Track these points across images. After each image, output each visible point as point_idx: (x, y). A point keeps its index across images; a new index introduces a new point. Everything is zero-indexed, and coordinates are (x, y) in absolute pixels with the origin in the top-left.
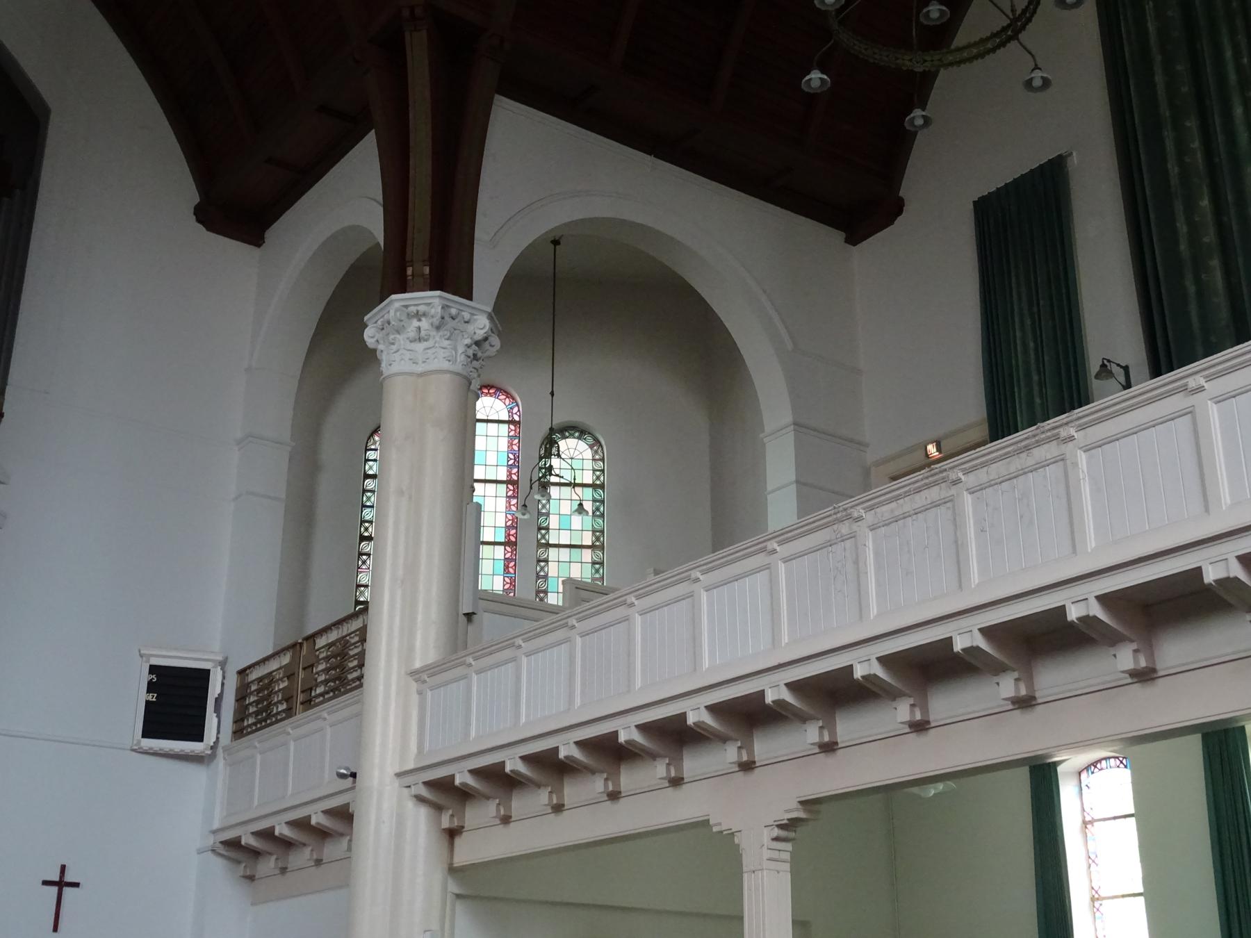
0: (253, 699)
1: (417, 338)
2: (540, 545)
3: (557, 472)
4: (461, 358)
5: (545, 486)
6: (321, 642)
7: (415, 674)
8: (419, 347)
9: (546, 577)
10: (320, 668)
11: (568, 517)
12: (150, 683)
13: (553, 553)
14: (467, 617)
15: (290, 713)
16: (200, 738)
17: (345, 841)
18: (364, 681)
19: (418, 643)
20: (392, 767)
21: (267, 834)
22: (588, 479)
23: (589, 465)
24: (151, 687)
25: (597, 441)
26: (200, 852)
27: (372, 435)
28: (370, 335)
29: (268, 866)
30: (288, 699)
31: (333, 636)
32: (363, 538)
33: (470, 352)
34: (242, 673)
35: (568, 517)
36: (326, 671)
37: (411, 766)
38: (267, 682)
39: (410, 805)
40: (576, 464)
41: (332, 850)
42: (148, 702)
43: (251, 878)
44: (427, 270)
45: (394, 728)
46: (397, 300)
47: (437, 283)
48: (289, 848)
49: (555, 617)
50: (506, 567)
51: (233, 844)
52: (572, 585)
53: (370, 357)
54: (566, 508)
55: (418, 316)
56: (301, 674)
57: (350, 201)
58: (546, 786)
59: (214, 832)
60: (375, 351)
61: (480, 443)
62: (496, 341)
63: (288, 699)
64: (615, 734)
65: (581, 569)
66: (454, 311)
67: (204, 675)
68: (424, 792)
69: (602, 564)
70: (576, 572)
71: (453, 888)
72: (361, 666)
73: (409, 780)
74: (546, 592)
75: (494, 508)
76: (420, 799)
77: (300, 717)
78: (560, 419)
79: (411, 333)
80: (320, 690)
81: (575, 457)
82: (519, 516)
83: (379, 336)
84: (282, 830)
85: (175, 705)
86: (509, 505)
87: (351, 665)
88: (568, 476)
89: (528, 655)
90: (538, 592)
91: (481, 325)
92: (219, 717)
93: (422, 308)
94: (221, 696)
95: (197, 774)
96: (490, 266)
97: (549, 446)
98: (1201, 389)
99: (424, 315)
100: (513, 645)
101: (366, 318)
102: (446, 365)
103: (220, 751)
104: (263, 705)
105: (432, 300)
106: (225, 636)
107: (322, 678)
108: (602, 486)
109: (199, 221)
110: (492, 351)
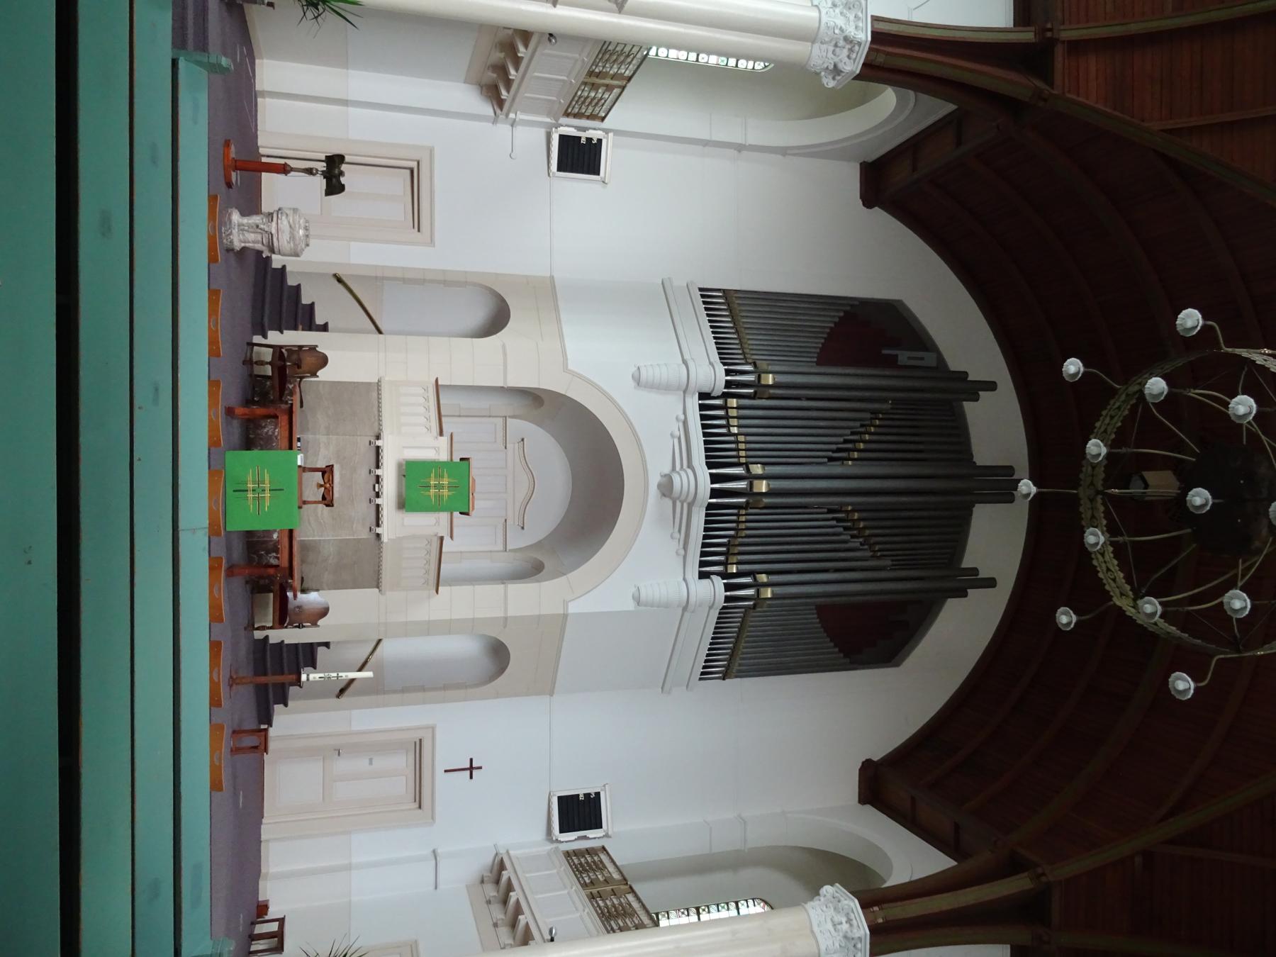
15: (584, 885)
24: (587, 795)
43: (482, 882)
51: (502, 866)
67: (598, 825)
85: (579, 812)
104: (586, 866)
106: (624, 835)
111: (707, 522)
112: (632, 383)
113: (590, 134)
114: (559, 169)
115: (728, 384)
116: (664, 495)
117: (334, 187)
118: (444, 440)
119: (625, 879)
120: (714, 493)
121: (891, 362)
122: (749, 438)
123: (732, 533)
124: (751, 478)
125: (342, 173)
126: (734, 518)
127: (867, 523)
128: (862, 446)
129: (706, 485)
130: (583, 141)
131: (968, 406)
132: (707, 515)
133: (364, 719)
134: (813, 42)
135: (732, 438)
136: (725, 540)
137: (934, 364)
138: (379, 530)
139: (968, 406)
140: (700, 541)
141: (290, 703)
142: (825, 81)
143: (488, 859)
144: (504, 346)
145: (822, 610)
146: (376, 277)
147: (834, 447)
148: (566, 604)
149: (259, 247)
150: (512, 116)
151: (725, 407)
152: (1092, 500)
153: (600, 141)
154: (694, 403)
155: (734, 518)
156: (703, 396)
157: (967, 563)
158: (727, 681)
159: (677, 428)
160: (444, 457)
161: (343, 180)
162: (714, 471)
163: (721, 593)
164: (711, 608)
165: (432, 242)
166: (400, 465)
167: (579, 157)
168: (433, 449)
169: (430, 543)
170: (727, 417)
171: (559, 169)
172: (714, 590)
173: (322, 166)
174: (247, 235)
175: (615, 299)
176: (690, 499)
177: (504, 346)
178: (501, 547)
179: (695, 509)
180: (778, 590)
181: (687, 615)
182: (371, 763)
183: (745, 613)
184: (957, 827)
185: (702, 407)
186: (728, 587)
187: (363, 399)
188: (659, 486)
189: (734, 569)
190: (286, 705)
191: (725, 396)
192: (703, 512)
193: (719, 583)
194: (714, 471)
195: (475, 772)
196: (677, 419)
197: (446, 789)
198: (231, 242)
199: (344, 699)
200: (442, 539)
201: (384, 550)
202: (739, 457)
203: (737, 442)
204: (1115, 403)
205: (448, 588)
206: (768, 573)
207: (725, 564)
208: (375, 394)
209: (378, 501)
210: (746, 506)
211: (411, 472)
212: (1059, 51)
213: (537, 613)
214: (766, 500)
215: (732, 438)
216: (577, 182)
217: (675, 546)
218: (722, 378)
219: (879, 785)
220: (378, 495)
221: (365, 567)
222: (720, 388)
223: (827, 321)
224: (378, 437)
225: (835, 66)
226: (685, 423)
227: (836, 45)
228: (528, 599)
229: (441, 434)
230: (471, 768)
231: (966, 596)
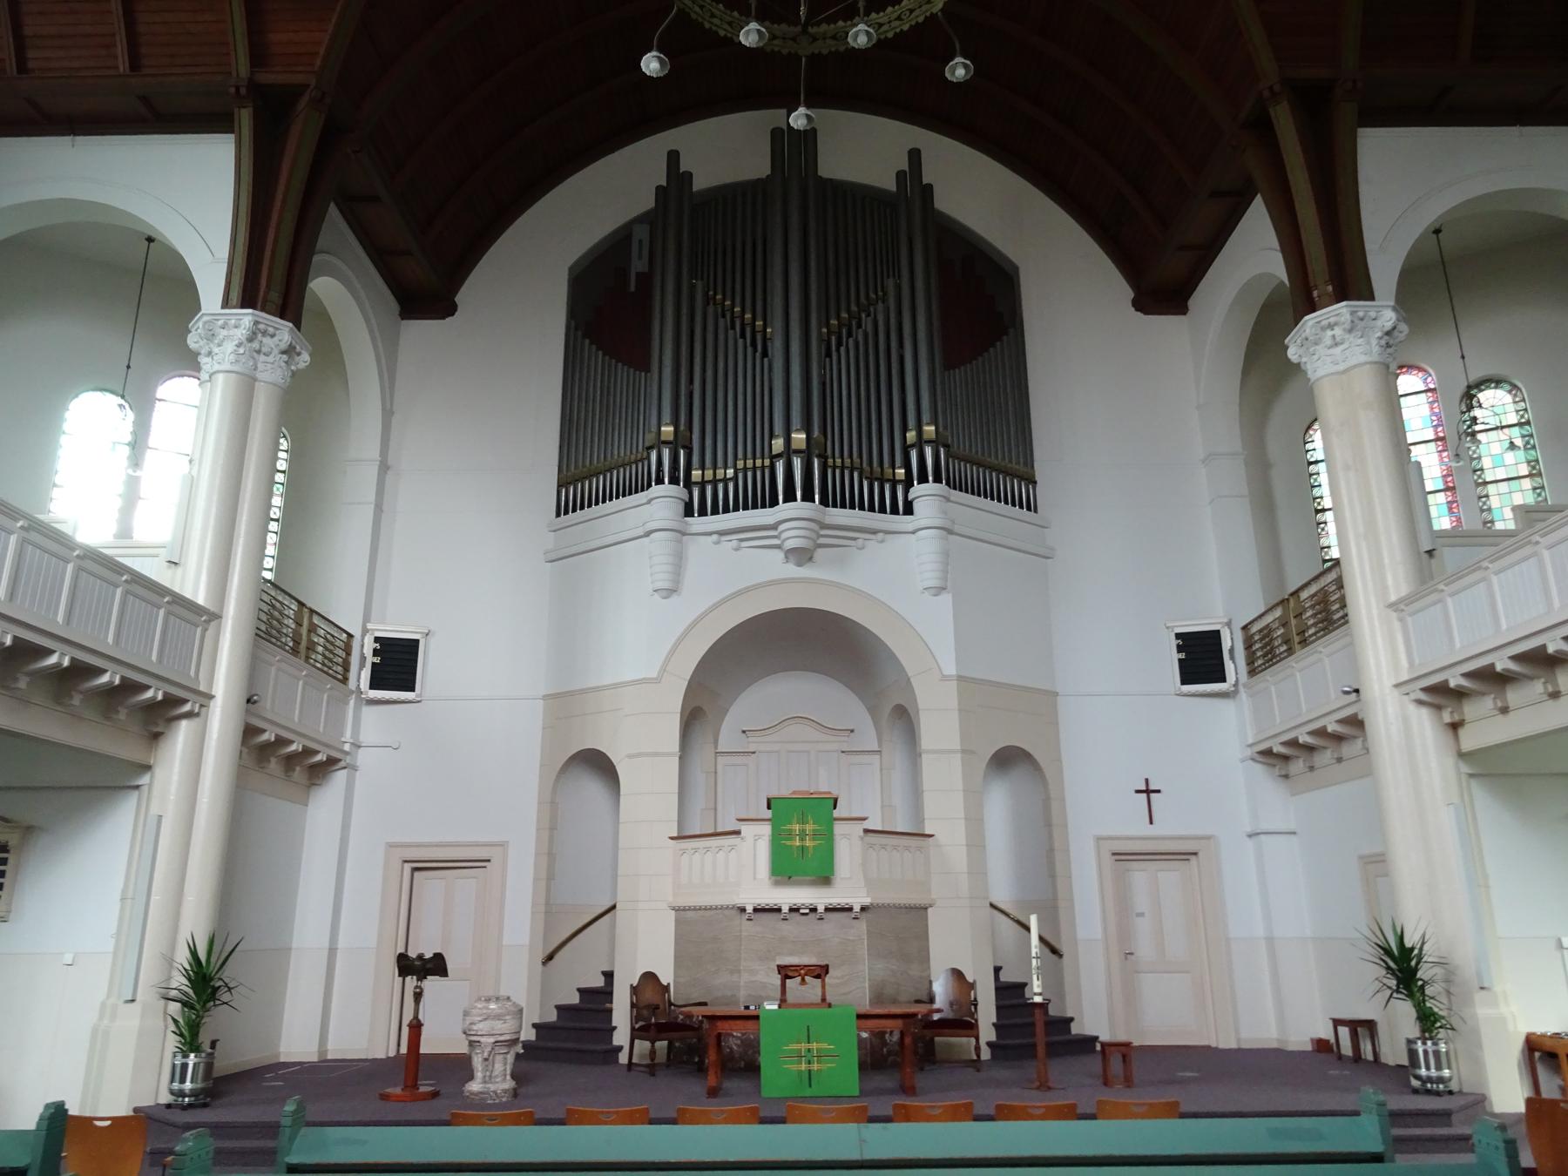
0: (1258, 646)
1: (1333, 345)
2: (1478, 485)
4: (1376, 349)
5: (1473, 434)
6: (1304, 595)
7: (1392, 606)
8: (1338, 350)
9: (1489, 509)
10: (1310, 612)
11: (1500, 455)
13: (1491, 489)
14: (1429, 557)
15: (1290, 651)
16: (1223, 680)
17: (1359, 742)
18: (1351, 617)
19: (1390, 581)
20: (1389, 682)
21: (1293, 743)
22: (1513, 419)
23: (1511, 407)
24: (1180, 649)
25: (1515, 387)
26: (1243, 761)
27: (1309, 427)
28: (1293, 353)
29: (1298, 766)
30: (1286, 642)
31: (1313, 589)
32: (1318, 511)
33: (1383, 342)
34: (1245, 628)
35: (1500, 455)
36: (1314, 616)
37: (1405, 677)
38: (1267, 632)
39: (1412, 709)
40: (1498, 410)
41: (1347, 750)
43: (1286, 776)
44: (1330, 288)
45: (1383, 652)
46: (1310, 320)
47: (1341, 295)
48: (1317, 751)
49: (1513, 540)
50: (1450, 509)
51: (1268, 753)
52: (1521, 511)
53: (1297, 368)
54: (1496, 449)
55: (1331, 326)
56: (1293, 622)
57: (1254, 253)
58: (1539, 678)
60: (1298, 365)
61: (1406, 414)
62: (1404, 327)
63: (1286, 642)
64: (1544, 647)
65: (1524, 494)
66: (1361, 314)
67: (1216, 635)
68: (1423, 696)
69: (1543, 488)
70: (1518, 500)
71: (1465, 769)
72: (1344, 606)
74: (1492, 522)
75: (1431, 463)
76: (1420, 702)
77: (1300, 652)
78: (1474, 376)
79: (1329, 342)
80: (1311, 631)
81: (1496, 404)
82: (1454, 464)
83: (1301, 351)
84: (1278, 749)
85: (1200, 658)
86: (1441, 459)
87: (1334, 608)
88: (1494, 422)
89: (1496, 574)
90: (1485, 523)
91: (1388, 318)
93: (1332, 320)
95: (1226, 706)
96: (1384, 267)
97: (1469, 398)
98: (1537, 543)
99: (1336, 324)
100: (1480, 568)
102: (1363, 359)
103: (1241, 688)
104: (1266, 650)
105: (1341, 311)
106: (1228, 603)
107: (1311, 622)
108: (1528, 423)
110: (1402, 337)
111: (843, 506)
112: (675, 598)
113: (368, 651)
114: (412, 689)
115: (674, 480)
116: (811, 559)
117: (436, 966)
118: (746, 829)
120: (809, 497)
121: (645, 280)
122: (740, 455)
124: (788, 453)
125: (420, 957)
127: (843, 306)
129: (798, 508)
130: (377, 660)
132: (835, 506)
138: (857, 908)
140: (866, 514)
141: (1069, 1014)
142: (302, 365)
144: (630, 756)
147: (750, 350)
148: (945, 678)
151: (702, 485)
153: (377, 639)
154: (697, 523)
156: (688, 512)
157: (890, 185)
159: (729, 543)
160: (766, 830)
161: (428, 955)
162: (781, 498)
163: (930, 487)
164: (948, 500)
165: (503, 845)
166: (777, 883)
167: (397, 664)
168: (757, 842)
169: (871, 846)
170: (715, 482)
171: (412, 689)
172: (926, 495)
174: (496, 1073)
175: (570, 619)
177: (630, 756)
179: (828, 520)
180: (926, 417)
181: (956, 528)
183: (954, 457)
185: (703, 513)
186: (923, 479)
187: (697, 928)
188: (799, 565)
189: (901, 472)
190: (1072, 1019)
191: (688, 484)
193: (917, 490)
194: (781, 498)
195: (1152, 787)
197: (1172, 824)
198: (505, 1091)
200: (867, 831)
201: (880, 902)
203: (745, 469)
206: (905, 429)
207: (894, 483)
208: (690, 914)
209: (821, 909)
210: (823, 457)
211: (784, 869)
212: (265, 78)
213: (956, 713)
215: (740, 476)
216: (428, 667)
217: (872, 544)
218: (666, 488)
219: (1163, 290)
220: (814, 910)
221: (903, 925)
222: (679, 491)
224: (743, 910)
225: (283, 352)
226: (722, 533)
227: (259, 352)
228: (940, 725)
229: (738, 833)
230: (1148, 792)
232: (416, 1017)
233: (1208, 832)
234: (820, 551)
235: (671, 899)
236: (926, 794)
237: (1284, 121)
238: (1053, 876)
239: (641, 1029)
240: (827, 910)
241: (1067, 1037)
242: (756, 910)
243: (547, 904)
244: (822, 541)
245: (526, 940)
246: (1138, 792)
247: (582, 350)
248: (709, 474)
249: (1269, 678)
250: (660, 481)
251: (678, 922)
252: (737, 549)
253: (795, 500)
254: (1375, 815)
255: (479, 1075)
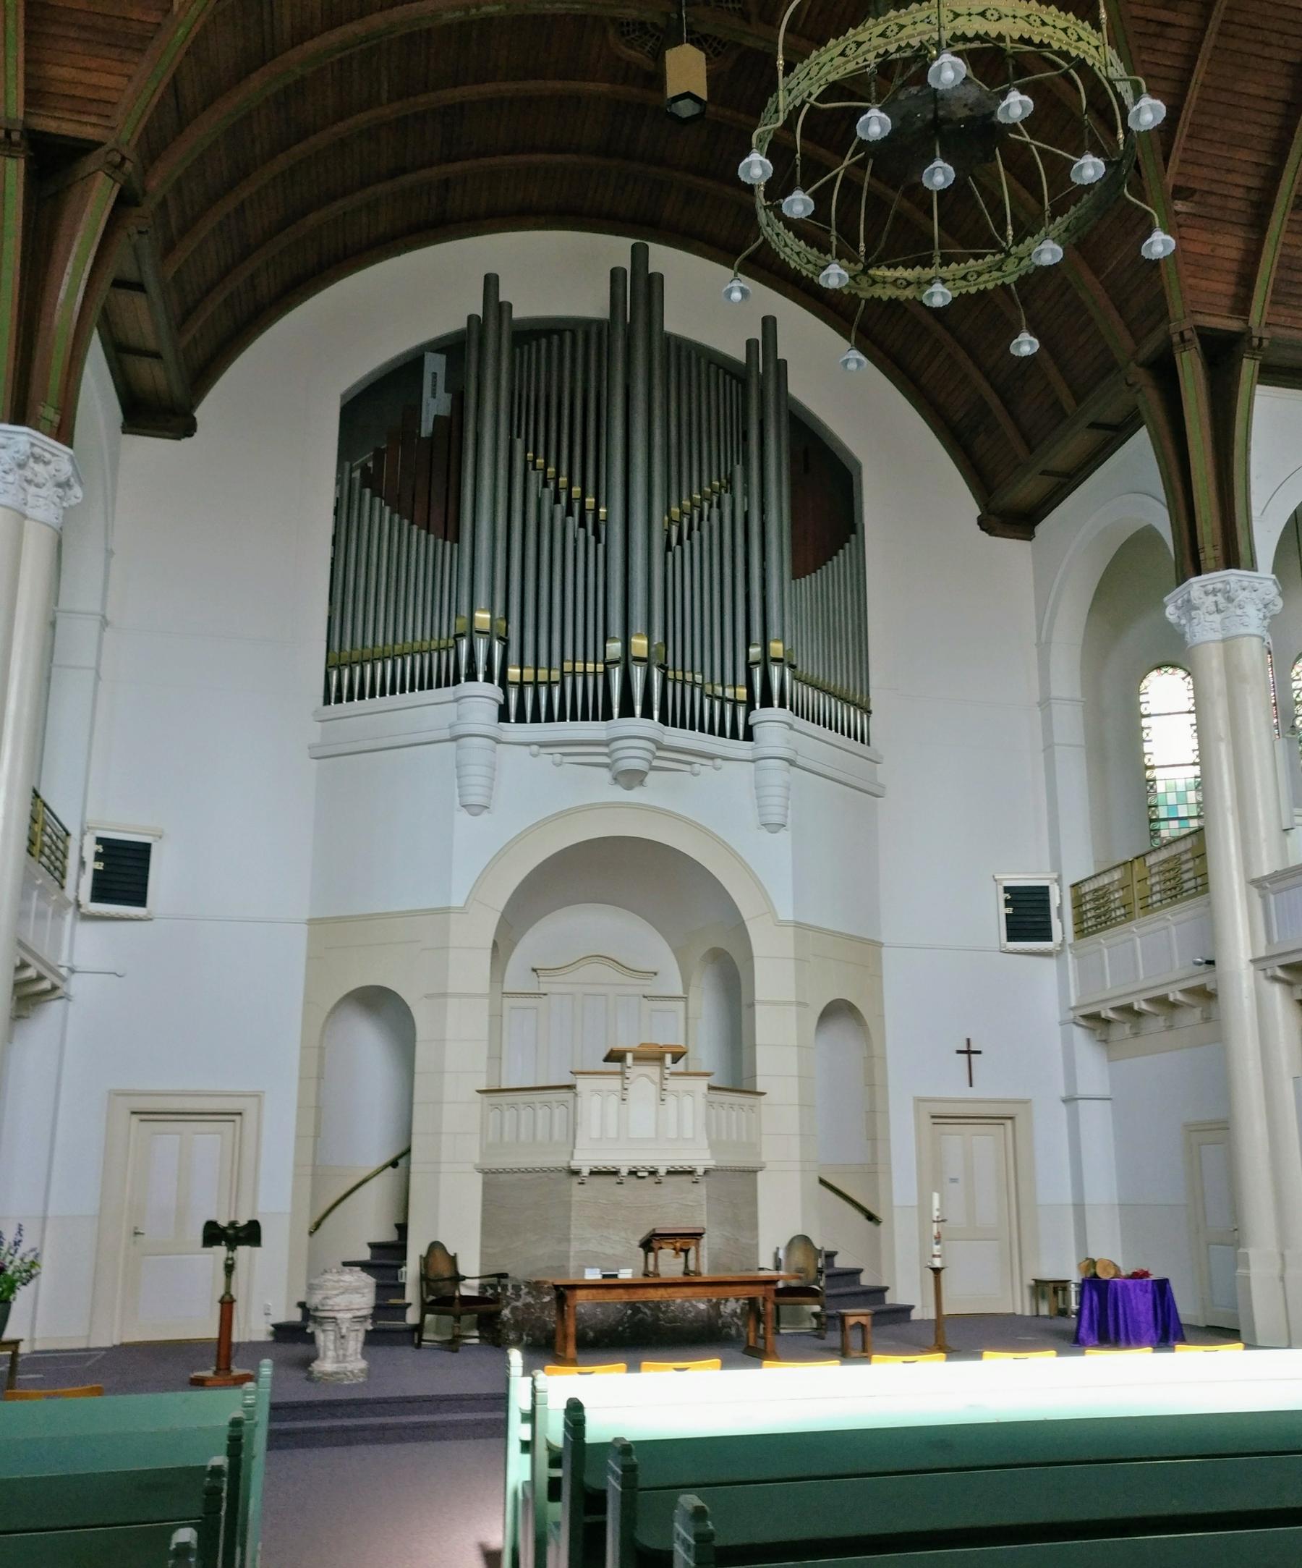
3: (42, 501)
12: (1006, 901)
15: (1129, 916)
16: (1049, 938)
33: (1261, 615)
42: (1007, 915)
43: (1105, 1041)
51: (1094, 1018)
56: (1137, 886)
59: (1072, 1009)
67: (1044, 891)
68: (1280, 973)
73: (1264, 965)
76: (1275, 979)
85: (1027, 915)
92: (1062, 921)
94: (1061, 904)
96: (1266, 534)
101: (1166, 599)
104: (1096, 912)
106: (1064, 861)
109: (982, 529)
111: (683, 726)
113: (89, 856)
115: (489, 678)
116: (641, 783)
117: (251, 1234)
119: (1125, 864)
120: (647, 713)
121: (452, 427)
122: (569, 656)
123: (697, 691)
124: (626, 660)
125: (233, 1224)
126: (679, 686)
127: (685, 496)
128: (576, 490)
129: (637, 724)
130: (100, 866)
131: (517, 314)
132: (674, 725)
133: (902, 1192)
134: (25, 517)
135: (569, 680)
136: (707, 702)
137: (442, 359)
138: (700, 1171)
139: (517, 314)
140: (706, 736)
141: (884, 1284)
142: (74, 501)
143: (1079, 1034)
145: (796, 575)
146: (313, 1175)
147: (592, 539)
148: (781, 924)
149: (361, 1336)
150: (64, 971)
151: (521, 685)
152: (874, 282)
153: (100, 841)
154: (513, 730)
155: (679, 686)
156: (503, 715)
157: (738, 353)
158: (872, 707)
159: (546, 759)
161: (242, 1222)
162: (616, 711)
163: (775, 712)
164: (791, 727)
165: (257, 1095)
170: (536, 684)
173: (221, 1251)
174: (350, 1351)
176: (652, 746)
178: (682, 1004)
179: (667, 741)
180: (774, 631)
181: (800, 761)
182: (954, 1180)
183: (799, 680)
184: (1094, 425)
185: (521, 718)
186: (767, 702)
189: (742, 693)
190: (887, 1289)
191: (504, 683)
192: (670, 729)
193: (759, 714)
194: (616, 711)
195: (973, 1049)
196: (535, 756)
197: (992, 1086)
198: (362, 1371)
199: (880, 1214)
200: (711, 1088)
202: (595, 673)
204: (776, 244)
205: (759, 1079)
206: (748, 644)
208: (503, 1177)
210: (663, 667)
212: (49, 125)
214: (658, 638)
215: (569, 680)
216: (162, 876)
217: (705, 770)
218: (480, 686)
219: (1011, 515)
220: (653, 1173)
222: (494, 690)
223: (379, 514)
225: (59, 485)
226: (542, 745)
227: (29, 482)
229: (571, 1087)
231: (785, 362)
232: (228, 1292)
233: (1028, 1097)
234: (652, 774)
235: (477, 1161)
236: (759, 1049)
237: (1190, 368)
238: (873, 1139)
239: (433, 1303)
240: (669, 1173)
241: (882, 1307)
242: (669, 1173)
243: (314, 1165)
244: (656, 763)
245: (287, 1207)
246: (959, 1052)
247: (361, 500)
248: (529, 675)
249: (1103, 941)
250: (472, 677)
251: (486, 1186)
252: (558, 765)
253: (633, 715)
254: (1220, 1083)
255: (331, 1354)
